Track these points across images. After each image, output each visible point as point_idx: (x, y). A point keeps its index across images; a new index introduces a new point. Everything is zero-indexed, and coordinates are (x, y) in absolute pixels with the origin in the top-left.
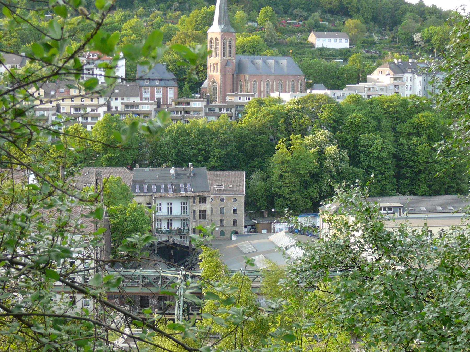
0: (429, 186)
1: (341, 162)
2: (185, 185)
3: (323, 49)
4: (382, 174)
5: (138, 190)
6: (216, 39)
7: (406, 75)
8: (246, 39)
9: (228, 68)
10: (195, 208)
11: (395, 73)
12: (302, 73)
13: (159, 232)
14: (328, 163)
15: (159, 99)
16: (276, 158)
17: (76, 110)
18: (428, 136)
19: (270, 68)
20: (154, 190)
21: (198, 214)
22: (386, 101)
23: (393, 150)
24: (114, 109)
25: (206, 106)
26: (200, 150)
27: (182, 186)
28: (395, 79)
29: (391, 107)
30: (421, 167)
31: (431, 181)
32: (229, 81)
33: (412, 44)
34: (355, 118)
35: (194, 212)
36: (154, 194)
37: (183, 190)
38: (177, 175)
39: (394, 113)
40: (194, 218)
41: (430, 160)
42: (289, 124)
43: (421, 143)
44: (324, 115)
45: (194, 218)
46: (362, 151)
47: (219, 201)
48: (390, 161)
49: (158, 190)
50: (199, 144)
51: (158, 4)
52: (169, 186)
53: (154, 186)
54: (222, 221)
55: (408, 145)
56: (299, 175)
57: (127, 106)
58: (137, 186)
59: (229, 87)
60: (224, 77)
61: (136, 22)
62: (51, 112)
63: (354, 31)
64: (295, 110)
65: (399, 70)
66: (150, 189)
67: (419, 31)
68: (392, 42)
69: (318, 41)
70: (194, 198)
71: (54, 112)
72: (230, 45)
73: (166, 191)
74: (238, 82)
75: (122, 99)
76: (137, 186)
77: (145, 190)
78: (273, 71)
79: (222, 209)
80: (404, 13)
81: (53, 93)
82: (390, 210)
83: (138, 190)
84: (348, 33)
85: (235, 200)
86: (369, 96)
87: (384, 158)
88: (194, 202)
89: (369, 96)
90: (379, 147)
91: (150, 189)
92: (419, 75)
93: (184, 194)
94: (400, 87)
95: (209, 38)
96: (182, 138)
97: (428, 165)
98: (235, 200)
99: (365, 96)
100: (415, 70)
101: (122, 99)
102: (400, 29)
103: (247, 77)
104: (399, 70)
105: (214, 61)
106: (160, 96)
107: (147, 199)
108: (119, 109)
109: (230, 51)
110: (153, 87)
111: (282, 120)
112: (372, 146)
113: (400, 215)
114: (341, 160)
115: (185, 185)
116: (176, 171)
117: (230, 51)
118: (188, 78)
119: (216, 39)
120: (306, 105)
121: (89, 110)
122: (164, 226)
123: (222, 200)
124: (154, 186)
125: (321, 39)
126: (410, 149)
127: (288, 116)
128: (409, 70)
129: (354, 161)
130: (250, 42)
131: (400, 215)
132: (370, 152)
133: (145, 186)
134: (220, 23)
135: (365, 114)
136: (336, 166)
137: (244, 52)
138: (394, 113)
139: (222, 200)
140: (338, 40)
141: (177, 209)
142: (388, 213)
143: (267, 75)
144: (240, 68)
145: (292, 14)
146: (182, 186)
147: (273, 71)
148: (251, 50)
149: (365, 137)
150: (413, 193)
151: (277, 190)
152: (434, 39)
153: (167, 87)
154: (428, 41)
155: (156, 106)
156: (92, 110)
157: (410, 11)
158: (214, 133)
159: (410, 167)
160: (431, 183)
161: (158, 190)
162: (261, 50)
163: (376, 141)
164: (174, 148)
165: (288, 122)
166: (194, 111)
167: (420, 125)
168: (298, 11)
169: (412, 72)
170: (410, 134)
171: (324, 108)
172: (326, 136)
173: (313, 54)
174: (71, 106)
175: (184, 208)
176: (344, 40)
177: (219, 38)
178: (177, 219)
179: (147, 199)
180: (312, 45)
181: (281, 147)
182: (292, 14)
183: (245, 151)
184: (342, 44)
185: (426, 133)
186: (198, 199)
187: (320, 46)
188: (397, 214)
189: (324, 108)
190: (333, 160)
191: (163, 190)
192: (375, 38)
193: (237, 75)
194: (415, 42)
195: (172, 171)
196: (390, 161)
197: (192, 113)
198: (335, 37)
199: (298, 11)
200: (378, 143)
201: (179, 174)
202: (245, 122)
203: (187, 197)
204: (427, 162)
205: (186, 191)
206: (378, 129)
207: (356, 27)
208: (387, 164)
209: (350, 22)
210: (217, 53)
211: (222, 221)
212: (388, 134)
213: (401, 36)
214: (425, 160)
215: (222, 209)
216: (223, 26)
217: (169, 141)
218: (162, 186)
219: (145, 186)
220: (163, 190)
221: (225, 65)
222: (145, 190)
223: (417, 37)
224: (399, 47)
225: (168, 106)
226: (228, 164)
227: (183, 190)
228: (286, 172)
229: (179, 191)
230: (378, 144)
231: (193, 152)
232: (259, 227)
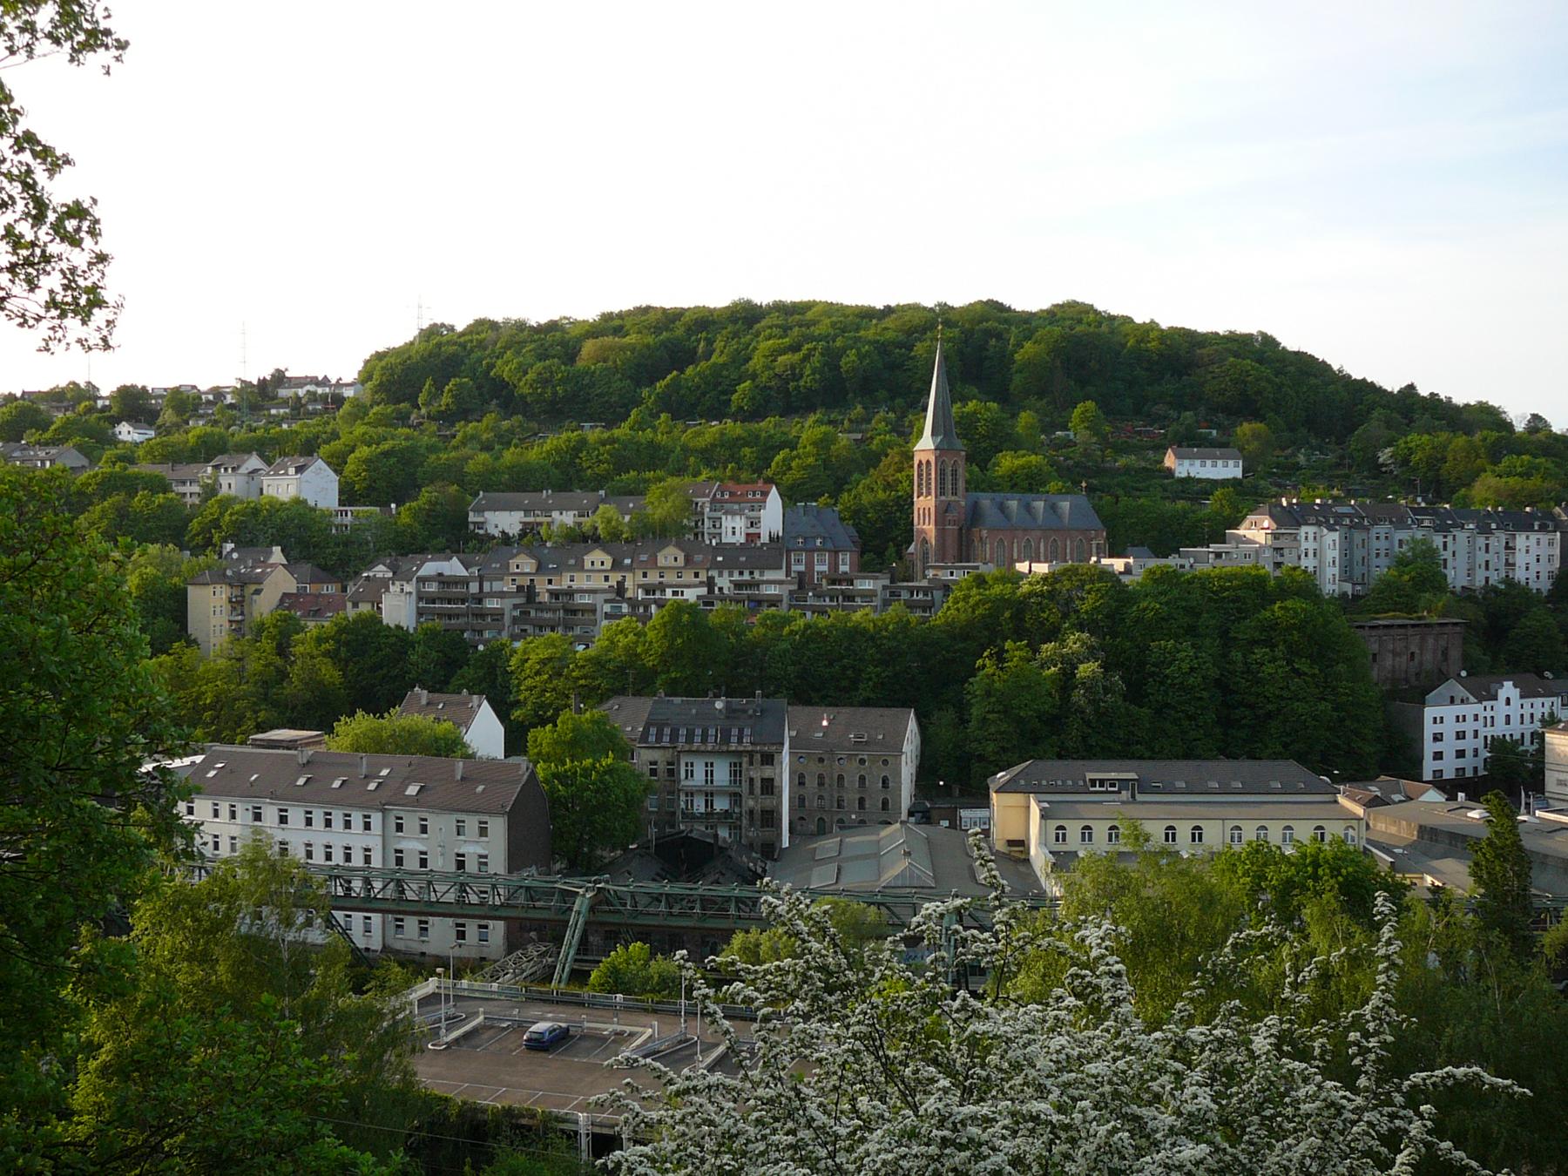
0: (1285, 746)
1: (1106, 694)
2: (741, 731)
3: (1189, 480)
4: (1190, 718)
5: (652, 739)
6: (928, 462)
7: (1304, 529)
9: (949, 516)
11: (1280, 524)
12: (1100, 525)
13: (689, 816)
16: (976, 684)
17: (647, 593)
19: (1060, 517)
20: (682, 739)
21: (758, 784)
22: (1220, 578)
23: (1214, 673)
25: (885, 587)
26: (844, 668)
27: (735, 731)
28: (1276, 536)
29: (1227, 589)
31: (1289, 735)
32: (951, 542)
33: (1376, 469)
34: (1145, 609)
35: (751, 780)
36: (680, 746)
37: (734, 739)
38: (730, 711)
39: (1233, 601)
40: (751, 792)
41: (1285, 694)
42: (1023, 618)
45: (751, 792)
46: (1152, 674)
47: (856, 764)
48: (1205, 694)
49: (690, 738)
51: (892, 399)
52: (712, 732)
53: (683, 731)
54: (861, 801)
57: (738, 585)
58: (653, 730)
59: (952, 551)
62: (600, 597)
63: (1253, 446)
64: (1037, 595)
65: (1289, 520)
66: (674, 736)
68: (1338, 465)
69: (1179, 465)
70: (751, 754)
73: (704, 740)
74: (970, 542)
76: (653, 730)
77: (666, 739)
78: (1040, 521)
79: (862, 778)
80: (1370, 409)
81: (628, 561)
82: (1113, 785)
83: (652, 739)
84: (1241, 449)
85: (885, 762)
86: (1278, 565)
88: (751, 763)
89: (1278, 565)
90: (1185, 667)
91: (674, 736)
92: (1331, 529)
94: (1286, 552)
96: (812, 646)
99: (1269, 568)
100: (1326, 519)
101: (731, 575)
102: (1353, 443)
103: (984, 534)
104: (1289, 520)
105: (925, 503)
107: (668, 754)
109: (955, 483)
111: (1007, 614)
112: (1170, 664)
113: (1133, 796)
114: (1106, 690)
115: (741, 731)
117: (955, 483)
118: (882, 538)
119: (928, 462)
121: (669, 592)
122: (699, 806)
123: (862, 761)
124: (683, 731)
125: (1186, 462)
126: (1249, 671)
127: (1020, 607)
128: (1312, 520)
131: (1133, 796)
132: (1167, 676)
133: (667, 731)
134: (933, 434)
135: (1167, 603)
138: (1233, 601)
139: (862, 761)
140: (1220, 462)
141: (722, 775)
143: (1025, 530)
144: (975, 516)
145: (1149, 416)
146: (735, 731)
150: (1252, 756)
152: (1415, 458)
153: (837, 553)
154: (1405, 462)
156: (675, 593)
157: (1384, 407)
158: (872, 638)
159: (1251, 707)
160: (1288, 740)
161: (690, 738)
162: (1044, 484)
163: (1179, 656)
165: (1018, 616)
166: (862, 596)
167: (1273, 626)
168: (1160, 409)
169: (1319, 524)
173: (1165, 490)
174: (639, 586)
175: (736, 773)
176: (1231, 463)
178: (722, 792)
179: (668, 754)
180: (1169, 473)
181: (987, 664)
182: (1149, 416)
184: (1230, 470)
187: (1184, 475)
191: (698, 739)
192: (1301, 459)
193: (969, 529)
194: (1383, 465)
195: (719, 705)
196: (1205, 694)
197: (858, 599)
198: (1214, 458)
199: (1160, 409)
200: (1182, 658)
201: (734, 711)
204: (1282, 698)
205: (740, 741)
206: (1191, 631)
207: (1256, 436)
209: (1246, 428)
210: (929, 489)
211: (861, 801)
212: (1208, 641)
213: (1356, 454)
215: (862, 778)
218: (698, 732)
219: (667, 731)
220: (698, 739)
221: (943, 512)
222: (666, 739)
223: (1384, 456)
224: (1347, 476)
226: (893, 696)
227: (734, 739)
228: (993, 712)
230: (1182, 660)
231: (829, 671)
232: (934, 814)
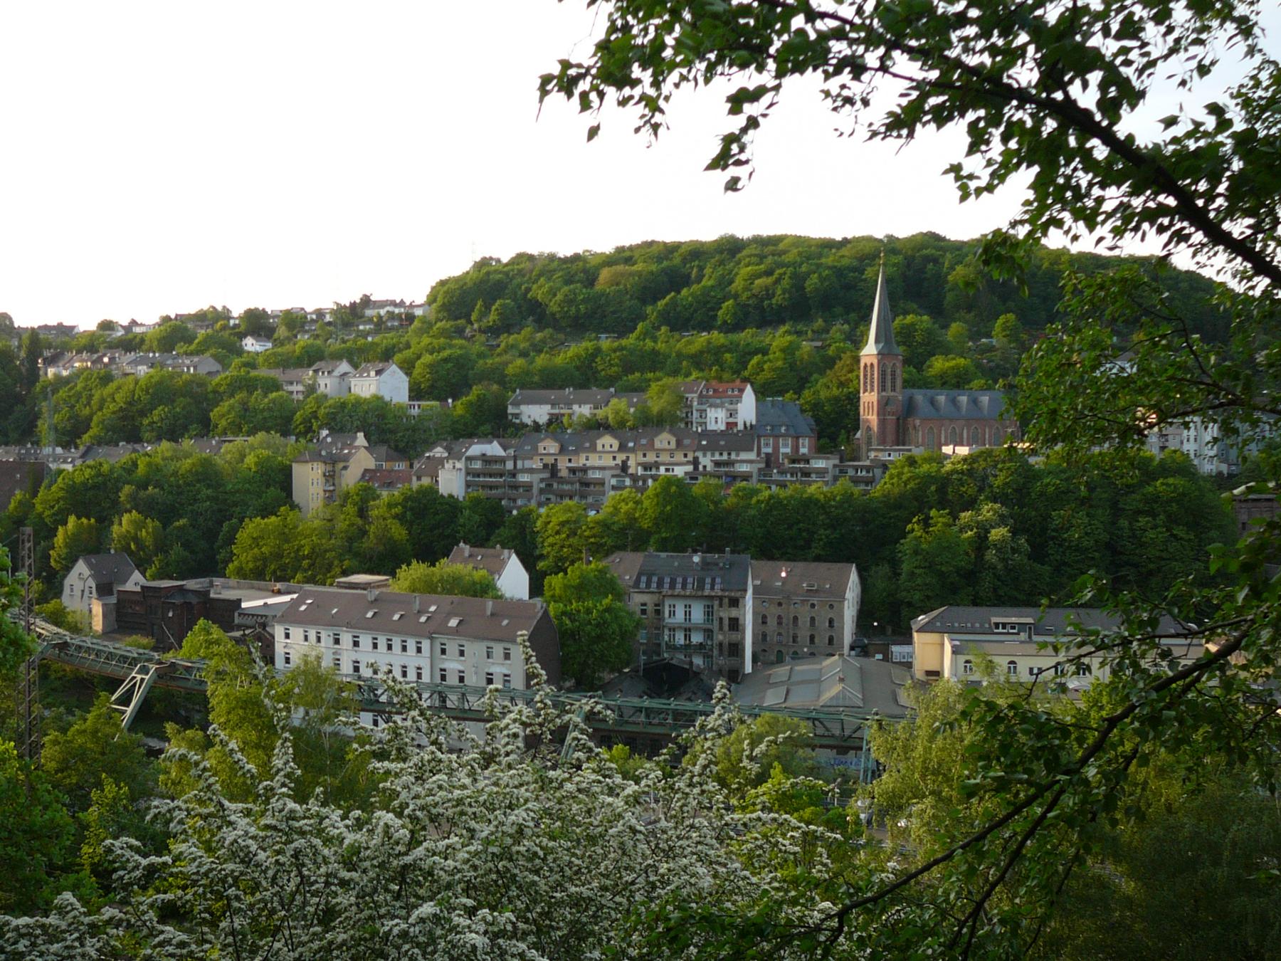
2: (713, 580)
5: (643, 585)
6: (872, 365)
8: (947, 364)
9: (889, 409)
10: (721, 614)
14: (991, 555)
15: (767, 454)
17: (645, 469)
18: (1169, 516)
20: (667, 586)
21: (726, 622)
23: (1105, 537)
24: (701, 468)
27: (708, 580)
30: (1151, 566)
32: (891, 428)
36: (666, 589)
38: (705, 565)
40: (721, 629)
41: (1164, 555)
43: (1155, 527)
44: (999, 480)
45: (721, 629)
46: (1053, 538)
49: (672, 586)
50: (799, 522)
52: (690, 580)
53: (667, 580)
54: (812, 638)
55: (1132, 530)
56: (941, 575)
57: (717, 464)
58: (644, 579)
60: (882, 422)
61: (791, 342)
62: (608, 473)
66: (660, 584)
67: (1265, 347)
70: (721, 598)
71: (618, 472)
72: (893, 374)
74: (905, 430)
75: (713, 455)
76: (644, 579)
79: (813, 619)
81: (631, 444)
82: (1013, 628)
83: (643, 585)
85: (831, 606)
87: (1087, 549)
88: (721, 605)
91: (660, 584)
93: (707, 593)
95: (862, 365)
97: (1163, 563)
98: (831, 606)
101: (713, 455)
103: (918, 422)
105: (869, 399)
106: (770, 450)
107: (655, 598)
108: (708, 469)
110: (777, 437)
111: (933, 488)
113: (1030, 637)
114: (1014, 550)
115: (713, 580)
116: (703, 559)
118: (835, 425)
119: (872, 365)
120: (975, 466)
123: (813, 606)
124: (667, 580)
126: (1134, 536)
127: (944, 483)
129: (1038, 553)
130: (953, 368)
131: (1030, 637)
132: (1065, 540)
133: (655, 579)
134: (877, 341)
136: (1004, 560)
137: (944, 384)
139: (813, 606)
141: (698, 614)
142: (1008, 633)
146: (708, 580)
147: (986, 412)
148: (954, 381)
149: (1059, 517)
151: (904, 594)
153: (798, 438)
155: (763, 465)
159: (1136, 566)
161: (672, 586)
164: (760, 526)
167: (1156, 498)
170: (1140, 512)
171: (1001, 470)
172: (996, 512)
175: (709, 613)
177: (875, 362)
179: (655, 598)
181: (915, 527)
183: (861, 535)
185: (1165, 512)
186: (726, 601)
188: (1023, 636)
189: (1001, 470)
190: (999, 550)
193: (905, 419)
195: (696, 559)
197: (813, 476)
202: (877, 490)
203: (711, 598)
204: (1162, 559)
205: (712, 588)
208: (1093, 558)
210: (872, 386)
211: (812, 638)
214: (1158, 554)
215: (813, 619)
216: (881, 346)
217: (754, 516)
218: (680, 580)
219: (655, 579)
225: (779, 466)
226: (838, 553)
229: (701, 586)
232: (871, 649)
